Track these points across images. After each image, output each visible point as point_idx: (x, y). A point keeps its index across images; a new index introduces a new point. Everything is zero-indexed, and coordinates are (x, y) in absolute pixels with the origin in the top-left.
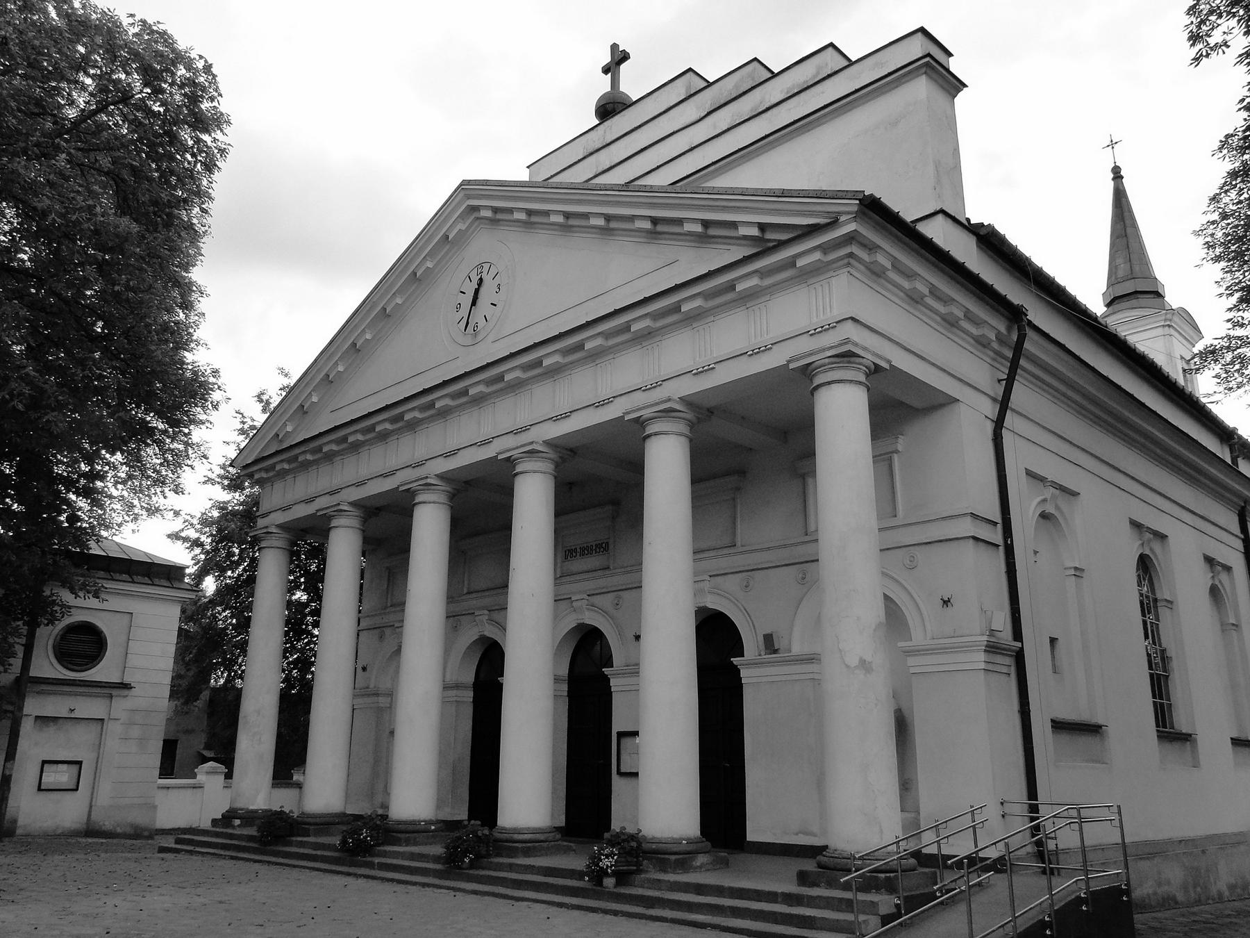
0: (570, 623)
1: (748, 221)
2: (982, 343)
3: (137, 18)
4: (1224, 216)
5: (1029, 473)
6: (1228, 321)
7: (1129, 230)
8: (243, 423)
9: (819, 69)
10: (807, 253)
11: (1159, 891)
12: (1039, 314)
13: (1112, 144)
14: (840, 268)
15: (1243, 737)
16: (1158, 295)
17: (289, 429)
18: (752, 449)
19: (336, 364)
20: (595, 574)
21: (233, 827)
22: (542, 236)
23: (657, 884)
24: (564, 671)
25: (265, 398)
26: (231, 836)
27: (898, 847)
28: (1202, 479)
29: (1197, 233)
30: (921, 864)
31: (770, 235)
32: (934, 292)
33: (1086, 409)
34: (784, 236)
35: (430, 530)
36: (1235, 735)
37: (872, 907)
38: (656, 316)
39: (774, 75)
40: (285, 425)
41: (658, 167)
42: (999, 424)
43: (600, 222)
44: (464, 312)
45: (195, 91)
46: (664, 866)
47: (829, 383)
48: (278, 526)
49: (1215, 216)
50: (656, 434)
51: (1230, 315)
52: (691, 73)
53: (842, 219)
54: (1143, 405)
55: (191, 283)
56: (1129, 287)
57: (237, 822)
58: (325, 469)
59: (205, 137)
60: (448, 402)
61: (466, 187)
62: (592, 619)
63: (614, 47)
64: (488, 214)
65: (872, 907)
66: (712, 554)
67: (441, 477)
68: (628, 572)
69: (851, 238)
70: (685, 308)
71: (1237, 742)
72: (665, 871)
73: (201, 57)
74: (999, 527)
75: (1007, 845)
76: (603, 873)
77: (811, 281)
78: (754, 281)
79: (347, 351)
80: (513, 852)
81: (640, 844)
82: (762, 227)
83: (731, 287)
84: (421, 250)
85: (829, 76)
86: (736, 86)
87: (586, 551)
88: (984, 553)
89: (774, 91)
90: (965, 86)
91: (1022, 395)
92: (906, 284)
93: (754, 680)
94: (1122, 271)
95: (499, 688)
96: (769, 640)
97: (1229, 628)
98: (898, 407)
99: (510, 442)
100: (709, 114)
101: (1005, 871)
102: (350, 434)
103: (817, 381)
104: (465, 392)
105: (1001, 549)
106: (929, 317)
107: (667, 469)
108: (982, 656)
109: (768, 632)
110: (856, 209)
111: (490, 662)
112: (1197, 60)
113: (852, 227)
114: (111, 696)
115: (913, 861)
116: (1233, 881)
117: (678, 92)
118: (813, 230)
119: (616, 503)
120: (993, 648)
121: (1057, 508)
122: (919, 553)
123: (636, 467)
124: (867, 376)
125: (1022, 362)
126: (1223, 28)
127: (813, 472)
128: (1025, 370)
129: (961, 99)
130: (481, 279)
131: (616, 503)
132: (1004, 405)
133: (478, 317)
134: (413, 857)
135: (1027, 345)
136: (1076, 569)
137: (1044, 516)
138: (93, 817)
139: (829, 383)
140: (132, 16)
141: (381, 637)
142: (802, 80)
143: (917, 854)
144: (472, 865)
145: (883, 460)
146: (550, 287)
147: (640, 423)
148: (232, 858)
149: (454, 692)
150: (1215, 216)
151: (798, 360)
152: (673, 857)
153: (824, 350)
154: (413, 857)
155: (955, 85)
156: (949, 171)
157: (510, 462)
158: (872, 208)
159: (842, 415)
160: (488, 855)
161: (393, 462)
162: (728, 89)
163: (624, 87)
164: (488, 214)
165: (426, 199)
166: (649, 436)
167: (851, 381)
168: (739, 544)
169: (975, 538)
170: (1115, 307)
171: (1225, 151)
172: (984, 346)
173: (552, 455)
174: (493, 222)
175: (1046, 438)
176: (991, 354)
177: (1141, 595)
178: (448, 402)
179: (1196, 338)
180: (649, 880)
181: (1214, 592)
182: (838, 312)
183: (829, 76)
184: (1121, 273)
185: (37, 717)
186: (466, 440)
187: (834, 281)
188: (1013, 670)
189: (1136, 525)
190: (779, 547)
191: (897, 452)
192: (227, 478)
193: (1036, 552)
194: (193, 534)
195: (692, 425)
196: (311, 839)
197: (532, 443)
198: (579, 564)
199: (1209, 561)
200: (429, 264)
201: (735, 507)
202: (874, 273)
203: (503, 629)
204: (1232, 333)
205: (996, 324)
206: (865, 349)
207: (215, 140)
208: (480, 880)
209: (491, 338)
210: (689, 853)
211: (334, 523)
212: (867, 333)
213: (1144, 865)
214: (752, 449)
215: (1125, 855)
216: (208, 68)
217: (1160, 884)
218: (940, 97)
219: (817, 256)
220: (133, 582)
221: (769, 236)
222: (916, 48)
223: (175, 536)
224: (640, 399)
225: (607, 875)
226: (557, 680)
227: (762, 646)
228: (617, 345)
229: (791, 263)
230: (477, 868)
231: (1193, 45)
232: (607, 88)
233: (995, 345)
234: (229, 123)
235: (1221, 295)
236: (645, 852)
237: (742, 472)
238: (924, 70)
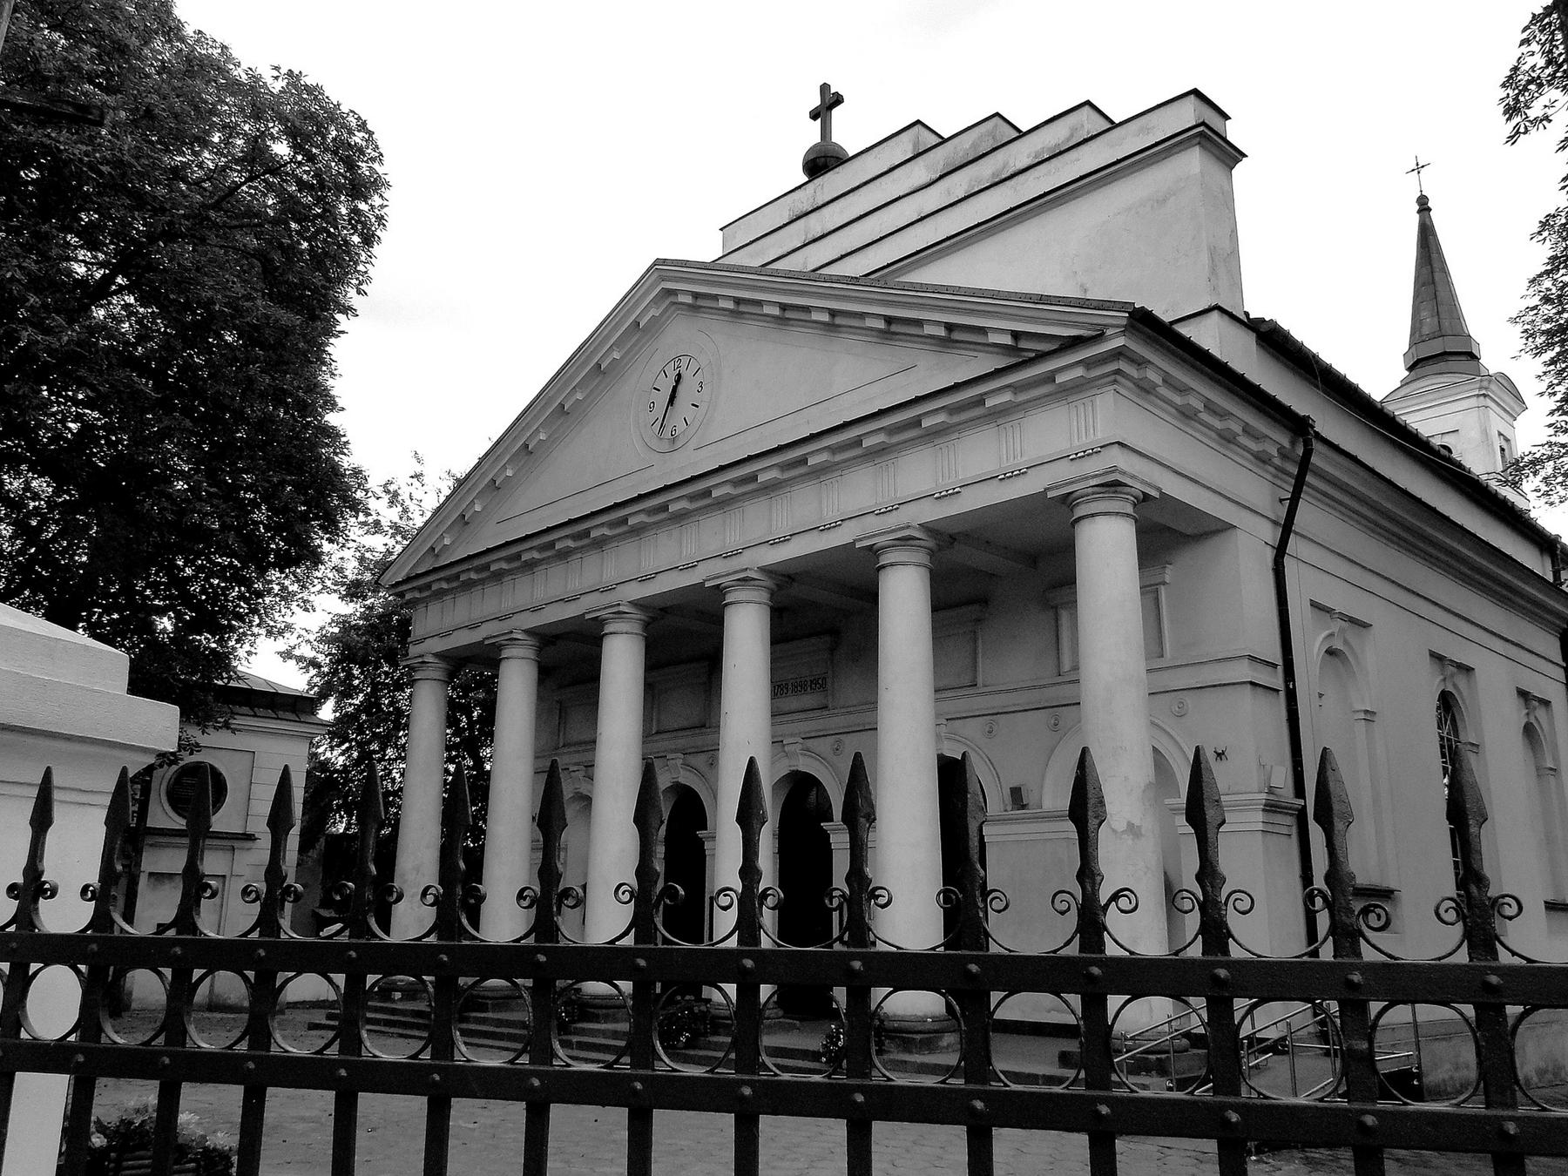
1: (1000, 328)
2: (1262, 459)
3: (284, 70)
4: (1547, 300)
5: (1314, 604)
6: (1550, 426)
7: (1437, 276)
9: (1074, 130)
10: (1068, 368)
11: (1456, 1075)
12: (1330, 423)
13: (1418, 168)
14: (1105, 385)
15: (1560, 900)
16: (1473, 357)
18: (1004, 577)
20: (811, 714)
21: (394, 1001)
22: (751, 328)
25: (392, 488)
26: (394, 1012)
28: (1518, 600)
29: (1514, 321)
30: (1193, 1046)
31: (1023, 344)
32: (1210, 407)
33: (1376, 524)
35: (622, 664)
36: (1550, 898)
38: (892, 430)
39: (1022, 135)
42: (1280, 551)
44: (659, 412)
45: (349, 155)
47: (1093, 515)
48: (436, 655)
49: (1536, 301)
51: (1552, 420)
52: (919, 127)
53: (1109, 332)
54: (1447, 519)
56: (1436, 347)
57: (398, 995)
58: (491, 590)
59: (363, 206)
61: (661, 268)
62: (806, 765)
63: (825, 88)
67: (634, 603)
68: (850, 713)
69: (1118, 354)
70: (926, 423)
71: (1551, 906)
72: (910, 1052)
74: (1280, 669)
75: (1289, 1024)
78: (1006, 397)
81: (882, 1021)
82: (1016, 335)
83: (980, 401)
84: (607, 337)
86: (974, 146)
87: (800, 687)
88: (1263, 699)
89: (1020, 155)
90: (1245, 156)
91: (1308, 515)
92: (1178, 400)
93: (999, 839)
94: (1429, 325)
96: (1016, 793)
97: (1546, 772)
98: (1166, 534)
99: (719, 567)
100: (941, 177)
101: (1287, 1053)
103: (1079, 512)
104: (664, 508)
105: (1282, 694)
107: (904, 602)
108: (1260, 816)
110: (1124, 322)
112: (1513, 138)
113: (1119, 342)
114: (233, 849)
115: (1185, 1041)
116: (1542, 1064)
117: (902, 149)
119: (835, 633)
120: (1272, 808)
121: (1346, 642)
122: (1189, 699)
123: (870, 596)
125: (1309, 478)
126: (1543, 100)
127: (1072, 603)
128: (1310, 486)
129: (1238, 170)
130: (679, 375)
131: (835, 633)
132: (1287, 528)
133: (676, 419)
135: (1313, 459)
136: (1366, 712)
137: (1331, 652)
138: (216, 990)
139: (1093, 515)
140: (277, 68)
142: (1053, 143)
143: (1187, 1035)
144: (690, 1044)
145: (1150, 591)
146: (765, 391)
147: (874, 552)
148: (401, 1036)
150: (1536, 301)
151: (1057, 488)
152: (918, 1037)
153: (1087, 478)
155: (1231, 156)
156: (1225, 259)
157: (719, 591)
158: (1143, 321)
159: (1107, 551)
160: (705, 1034)
161: (575, 584)
162: (965, 146)
163: (837, 137)
166: (883, 567)
168: (980, 681)
169: (1252, 683)
170: (1419, 371)
171: (1545, 234)
172: (1264, 462)
173: (769, 583)
175: (1336, 563)
176: (1272, 470)
177: (1442, 738)
178: (643, 518)
179: (1518, 409)
180: (893, 1061)
181: (1529, 731)
182: (1102, 435)
184: (1426, 330)
185: (151, 874)
186: (668, 562)
187: (1098, 399)
188: (1294, 831)
189: (1437, 657)
190: (1029, 688)
191: (1164, 583)
192: (343, 584)
193: (1321, 695)
194: (306, 651)
195: (932, 553)
196: (490, 1015)
198: (792, 702)
199: (1523, 694)
200: (616, 355)
201: (975, 641)
204: (1553, 439)
206: (1133, 477)
209: (692, 444)
210: (936, 1031)
211: (505, 654)
212: (1135, 459)
213: (1440, 1047)
214: (1004, 577)
215: (1417, 1036)
216: (363, 126)
217: (1457, 1068)
218: (1215, 169)
219: (1079, 372)
220: (255, 716)
221: (1023, 344)
222: (1187, 115)
223: (287, 655)
224: (873, 524)
227: (1008, 799)
228: (845, 461)
229: (1050, 378)
230: (694, 1048)
231: (1509, 119)
232: (816, 138)
233: (1277, 461)
235: (1542, 394)
236: (886, 1030)
237: (983, 601)
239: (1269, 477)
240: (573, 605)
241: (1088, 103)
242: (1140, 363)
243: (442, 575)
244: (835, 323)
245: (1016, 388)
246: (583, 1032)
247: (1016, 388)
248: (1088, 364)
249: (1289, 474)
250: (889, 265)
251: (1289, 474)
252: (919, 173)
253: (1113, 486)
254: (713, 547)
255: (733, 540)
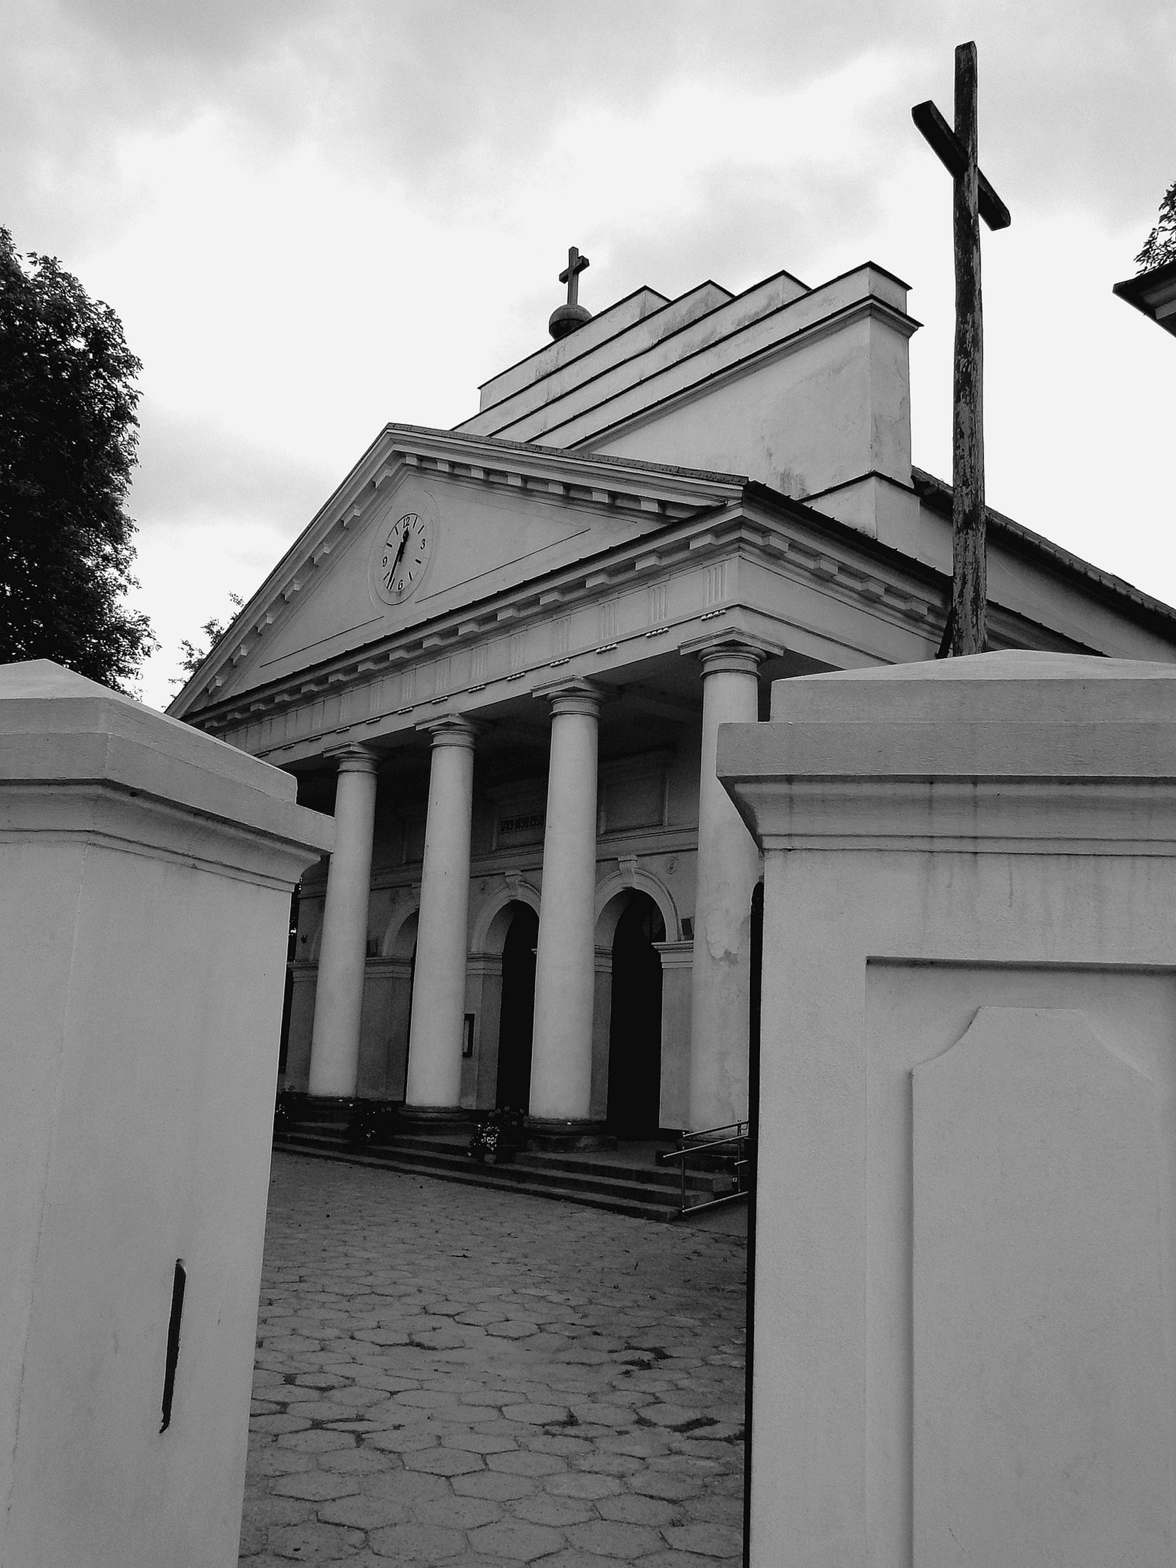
0: (615, 887)
2: (912, 618)
8: (191, 655)
9: (771, 299)
10: (699, 535)
17: (219, 683)
19: (265, 615)
23: (535, 1162)
24: (608, 943)
27: (739, 1130)
31: (670, 513)
34: (684, 515)
37: (706, 1185)
40: (214, 679)
41: (607, 401)
43: (518, 482)
45: (99, 340)
46: (545, 1146)
47: (716, 672)
50: (561, 713)
52: (646, 292)
53: (730, 503)
55: (121, 517)
60: (370, 666)
61: (393, 432)
62: (637, 883)
63: (573, 251)
64: (414, 462)
65: (706, 1185)
66: (640, 832)
67: (363, 744)
69: (740, 523)
72: (547, 1151)
73: (101, 303)
76: (485, 1148)
77: (706, 563)
79: (274, 603)
80: (417, 1130)
82: (663, 504)
83: (630, 565)
84: (348, 496)
85: (778, 310)
86: (690, 312)
89: (726, 322)
92: (811, 564)
95: (532, 960)
100: (660, 342)
102: (278, 693)
106: (842, 594)
109: (685, 917)
111: (521, 926)
113: (738, 513)
118: (704, 513)
124: (759, 664)
130: (407, 533)
133: (403, 575)
134: (324, 1132)
139: (716, 672)
140: (33, 255)
141: (393, 900)
146: (478, 547)
149: (481, 965)
154: (324, 1132)
158: (756, 494)
164: (414, 462)
165: (335, 457)
166: (555, 715)
167: (738, 671)
174: (420, 469)
182: (728, 599)
183: (778, 310)
195: (599, 703)
197: (447, 716)
200: (357, 512)
202: (770, 555)
203: (537, 889)
205: (925, 599)
206: (753, 637)
207: (126, 386)
208: (379, 1155)
209: (413, 599)
210: (573, 1133)
216: (110, 313)
219: (708, 539)
222: (860, 288)
224: (548, 675)
225: (490, 1152)
226: (599, 953)
229: (684, 545)
233: (931, 619)
234: (140, 366)
238: (868, 312)
239: (924, 634)
240: (315, 745)
241: (784, 273)
242: (765, 532)
243: (211, 714)
244: (528, 488)
245: (661, 553)
246: (300, 1129)
247: (661, 553)
248: (717, 532)
249: (939, 628)
250: (610, 427)
251: (939, 628)
252: (643, 337)
253: (733, 646)
254: (426, 694)
255: (441, 687)
